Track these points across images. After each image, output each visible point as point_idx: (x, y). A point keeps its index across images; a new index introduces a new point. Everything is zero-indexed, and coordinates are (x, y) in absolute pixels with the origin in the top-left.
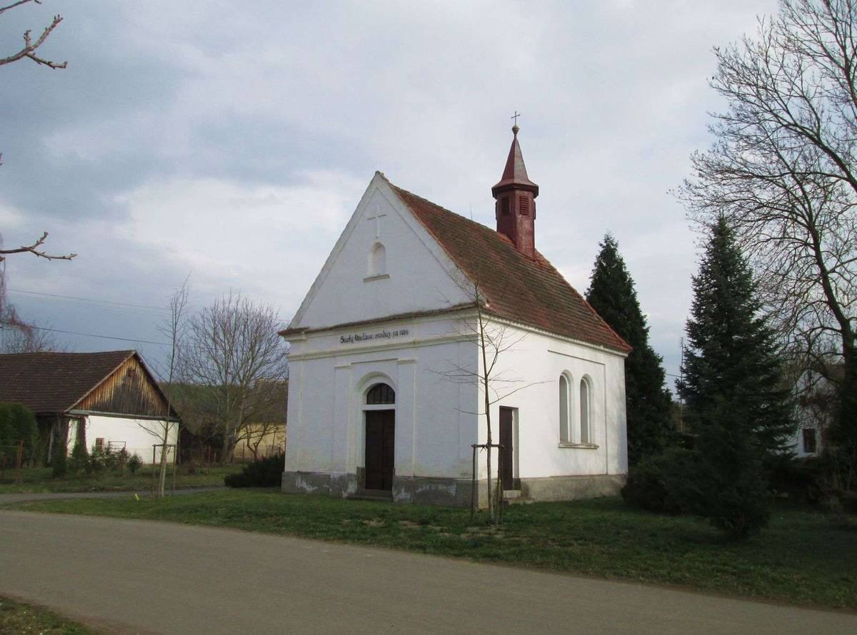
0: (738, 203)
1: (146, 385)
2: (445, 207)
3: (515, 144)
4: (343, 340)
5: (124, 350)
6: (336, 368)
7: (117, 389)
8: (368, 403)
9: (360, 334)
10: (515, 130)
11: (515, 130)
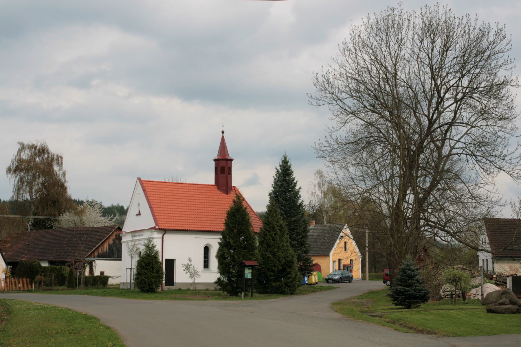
3: (223, 137)
7: (110, 245)
10: (223, 132)
11: (223, 132)
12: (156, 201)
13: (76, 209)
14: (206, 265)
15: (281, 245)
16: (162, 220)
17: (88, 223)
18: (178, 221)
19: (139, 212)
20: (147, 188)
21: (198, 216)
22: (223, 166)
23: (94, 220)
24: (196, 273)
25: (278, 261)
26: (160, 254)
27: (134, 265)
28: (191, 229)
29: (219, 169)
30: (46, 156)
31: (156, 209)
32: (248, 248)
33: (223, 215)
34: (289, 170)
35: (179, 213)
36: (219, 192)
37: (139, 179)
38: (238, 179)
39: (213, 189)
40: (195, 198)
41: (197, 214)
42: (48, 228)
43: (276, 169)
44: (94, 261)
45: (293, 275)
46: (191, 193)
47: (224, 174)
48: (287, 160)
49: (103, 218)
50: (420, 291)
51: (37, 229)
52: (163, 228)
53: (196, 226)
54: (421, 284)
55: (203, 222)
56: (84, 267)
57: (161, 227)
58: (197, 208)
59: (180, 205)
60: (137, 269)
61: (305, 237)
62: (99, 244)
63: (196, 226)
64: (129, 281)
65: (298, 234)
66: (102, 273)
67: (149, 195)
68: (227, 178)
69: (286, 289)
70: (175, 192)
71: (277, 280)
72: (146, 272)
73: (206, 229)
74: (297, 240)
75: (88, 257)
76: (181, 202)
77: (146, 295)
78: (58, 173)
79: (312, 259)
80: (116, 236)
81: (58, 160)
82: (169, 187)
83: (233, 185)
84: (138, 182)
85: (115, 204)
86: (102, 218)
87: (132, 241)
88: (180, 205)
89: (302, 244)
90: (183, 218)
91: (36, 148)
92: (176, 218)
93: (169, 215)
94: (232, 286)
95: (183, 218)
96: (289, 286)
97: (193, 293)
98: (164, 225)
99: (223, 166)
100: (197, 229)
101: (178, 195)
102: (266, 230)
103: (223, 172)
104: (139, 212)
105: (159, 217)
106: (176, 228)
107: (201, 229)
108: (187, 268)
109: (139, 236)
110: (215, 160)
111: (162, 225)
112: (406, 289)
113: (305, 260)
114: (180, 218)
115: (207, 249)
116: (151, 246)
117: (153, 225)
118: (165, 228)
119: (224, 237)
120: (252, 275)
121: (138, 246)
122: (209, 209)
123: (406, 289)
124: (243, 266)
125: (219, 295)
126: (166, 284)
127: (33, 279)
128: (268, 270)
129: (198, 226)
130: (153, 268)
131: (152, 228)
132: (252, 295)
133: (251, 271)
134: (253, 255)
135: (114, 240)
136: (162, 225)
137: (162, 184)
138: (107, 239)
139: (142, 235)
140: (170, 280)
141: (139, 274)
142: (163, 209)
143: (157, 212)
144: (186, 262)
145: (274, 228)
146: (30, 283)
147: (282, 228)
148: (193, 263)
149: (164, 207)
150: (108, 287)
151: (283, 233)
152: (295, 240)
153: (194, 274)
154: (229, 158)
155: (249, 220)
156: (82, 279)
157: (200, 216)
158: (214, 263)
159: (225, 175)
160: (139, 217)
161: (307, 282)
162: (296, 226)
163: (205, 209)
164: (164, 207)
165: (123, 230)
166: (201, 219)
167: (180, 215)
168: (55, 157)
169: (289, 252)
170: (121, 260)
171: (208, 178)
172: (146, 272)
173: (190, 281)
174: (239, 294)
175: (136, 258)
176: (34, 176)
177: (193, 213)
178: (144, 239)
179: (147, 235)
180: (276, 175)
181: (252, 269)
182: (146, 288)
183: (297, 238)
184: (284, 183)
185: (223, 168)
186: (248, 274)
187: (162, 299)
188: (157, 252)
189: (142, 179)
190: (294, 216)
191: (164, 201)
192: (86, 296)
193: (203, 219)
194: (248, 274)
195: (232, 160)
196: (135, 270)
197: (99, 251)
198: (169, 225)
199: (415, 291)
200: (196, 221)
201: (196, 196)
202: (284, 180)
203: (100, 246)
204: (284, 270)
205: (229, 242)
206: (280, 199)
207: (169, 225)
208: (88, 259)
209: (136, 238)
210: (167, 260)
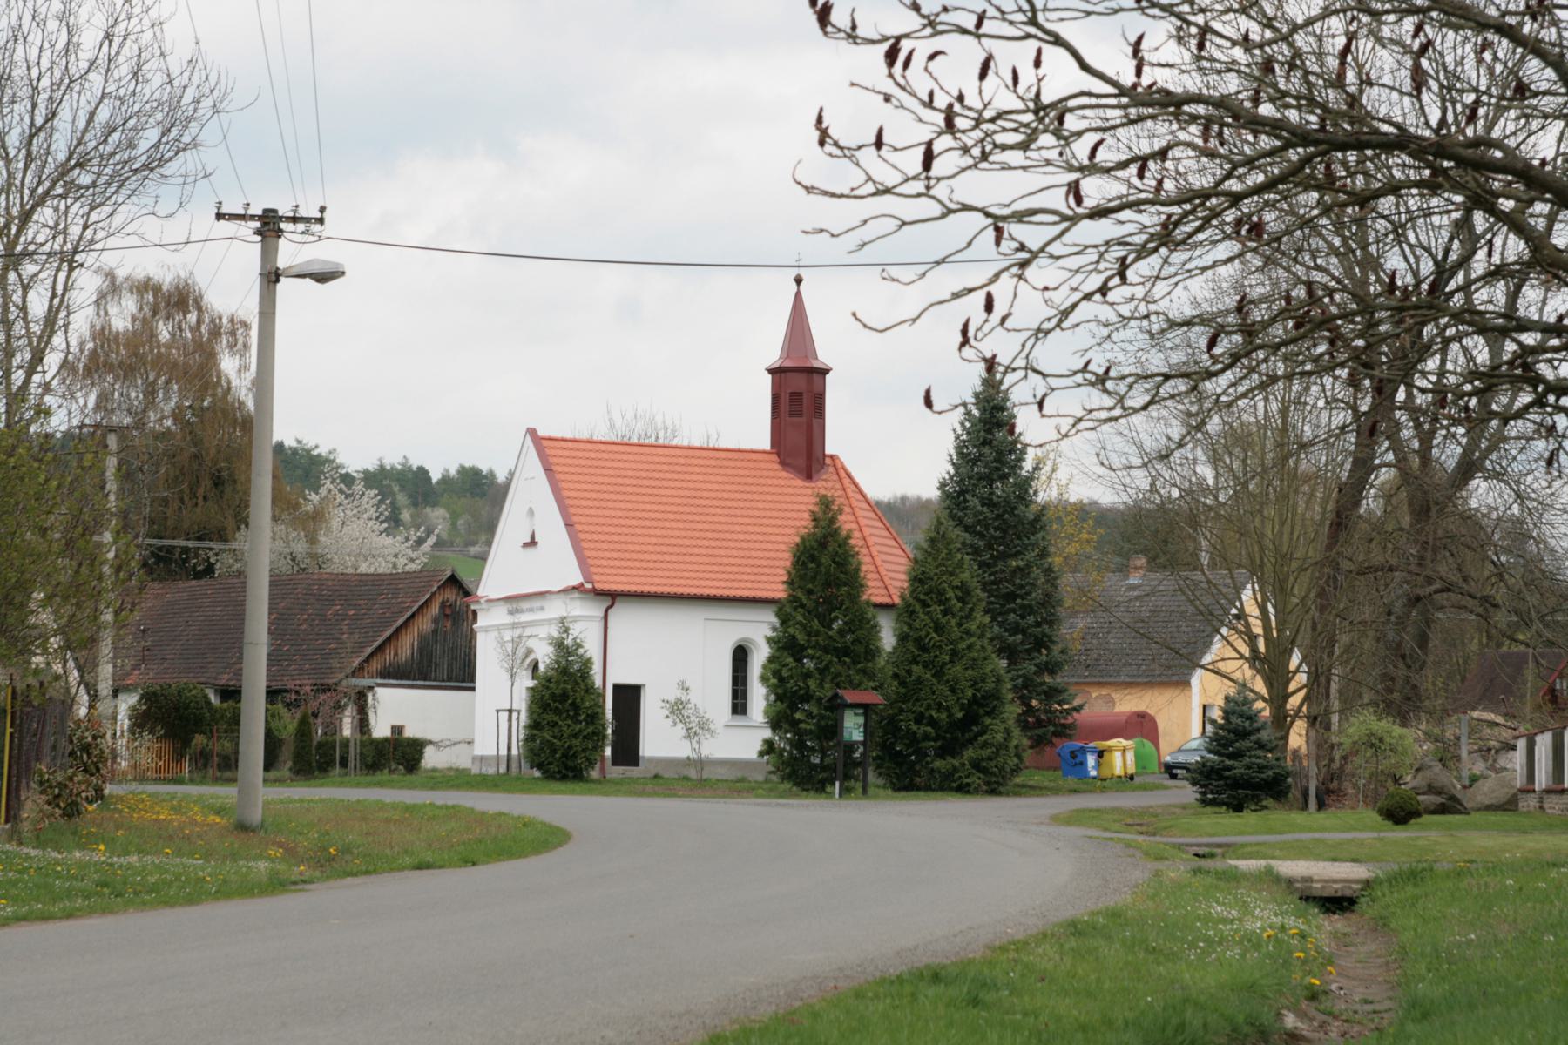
0: (435, 609)
3: (798, 294)
12: (584, 503)
13: (297, 506)
14: (739, 705)
15: (962, 645)
16: (604, 563)
17: (336, 559)
18: (651, 565)
19: (533, 536)
20: (555, 460)
21: (716, 552)
22: (799, 392)
23: (362, 544)
24: (704, 725)
25: (953, 690)
26: (596, 670)
27: (521, 702)
28: (693, 591)
29: (785, 399)
30: (192, 318)
31: (585, 528)
32: (859, 649)
33: (781, 555)
34: (1002, 409)
35: (654, 540)
36: (784, 474)
37: (532, 432)
38: (844, 431)
39: (763, 465)
40: (706, 494)
41: (713, 543)
42: (198, 575)
44: (371, 688)
45: (999, 737)
46: (694, 477)
47: (800, 415)
49: (389, 540)
50: (1261, 769)
51: (162, 580)
52: (606, 587)
53: (709, 583)
54: (1270, 751)
55: (729, 569)
56: (339, 707)
57: (599, 586)
58: (713, 527)
59: (659, 516)
60: (531, 711)
61: (1052, 621)
62: (388, 633)
63: (709, 583)
64: (503, 752)
65: (1027, 610)
66: (397, 730)
67: (563, 485)
68: (810, 428)
69: (975, 779)
70: (643, 474)
71: (946, 751)
72: (556, 718)
73: (738, 593)
74: (1023, 632)
75: (354, 674)
76: (662, 508)
78: (235, 383)
79: (1072, 690)
81: (233, 333)
82: (625, 457)
84: (529, 441)
85: (393, 460)
86: (386, 541)
87: (514, 626)
88: (659, 516)
89: (1041, 643)
90: (667, 558)
91: (157, 289)
92: (647, 557)
93: (624, 547)
94: (807, 760)
95: (667, 558)
96: (984, 771)
97: (694, 779)
98: (611, 579)
99: (799, 392)
100: (713, 592)
101: (653, 483)
102: (916, 598)
103: (796, 410)
104: (533, 536)
105: (594, 554)
106: (647, 589)
107: (725, 593)
108: (677, 709)
109: (531, 610)
110: (772, 371)
111: (603, 578)
112: (1228, 762)
113: (1045, 693)
114: (660, 557)
115: (741, 656)
116: (569, 642)
117: (576, 578)
118: (613, 587)
119: (785, 620)
120: (865, 732)
121: (531, 643)
122: (750, 529)
123: (1228, 762)
124: (836, 706)
126: (616, 761)
127: (186, 743)
128: (919, 720)
129: (717, 584)
130: (575, 707)
132: (865, 791)
133: (861, 720)
134: (871, 676)
135: (435, 620)
136: (603, 578)
137: (602, 447)
138: (413, 616)
139: (542, 609)
140: (628, 751)
141: (535, 726)
142: (605, 529)
143: (589, 537)
144: (674, 694)
145: (941, 593)
146: (179, 757)
147: (968, 593)
148: (694, 697)
149: (609, 521)
151: (972, 610)
152: (1015, 629)
153: (697, 728)
154: (816, 364)
155: (858, 570)
156: (352, 750)
157: (722, 552)
158: (758, 696)
159: (803, 420)
160: (530, 551)
161: (1093, 773)
162: (1022, 587)
163: (737, 528)
164: (609, 521)
165: (480, 593)
166: (726, 561)
167: (658, 549)
168: (225, 321)
169: (990, 667)
170: (473, 689)
171: (752, 428)
172: (556, 718)
174: (829, 789)
175: (526, 682)
176: (150, 392)
177: (699, 542)
178: (549, 622)
179: (556, 609)
180: (962, 424)
181: (866, 715)
182: (553, 768)
183: (1023, 623)
184: (986, 450)
185: (796, 397)
186: (853, 728)
187: (606, 794)
188: (587, 663)
189: (541, 433)
190: (1016, 555)
191: (610, 505)
193: (733, 561)
194: (853, 728)
195: (824, 372)
196: (524, 716)
197: (389, 656)
198: (624, 579)
199: (1248, 767)
200: (710, 568)
201: (709, 486)
202: (985, 443)
203: (389, 639)
204: (971, 719)
206: (974, 502)
207: (624, 579)
209: (524, 618)
210: (618, 688)
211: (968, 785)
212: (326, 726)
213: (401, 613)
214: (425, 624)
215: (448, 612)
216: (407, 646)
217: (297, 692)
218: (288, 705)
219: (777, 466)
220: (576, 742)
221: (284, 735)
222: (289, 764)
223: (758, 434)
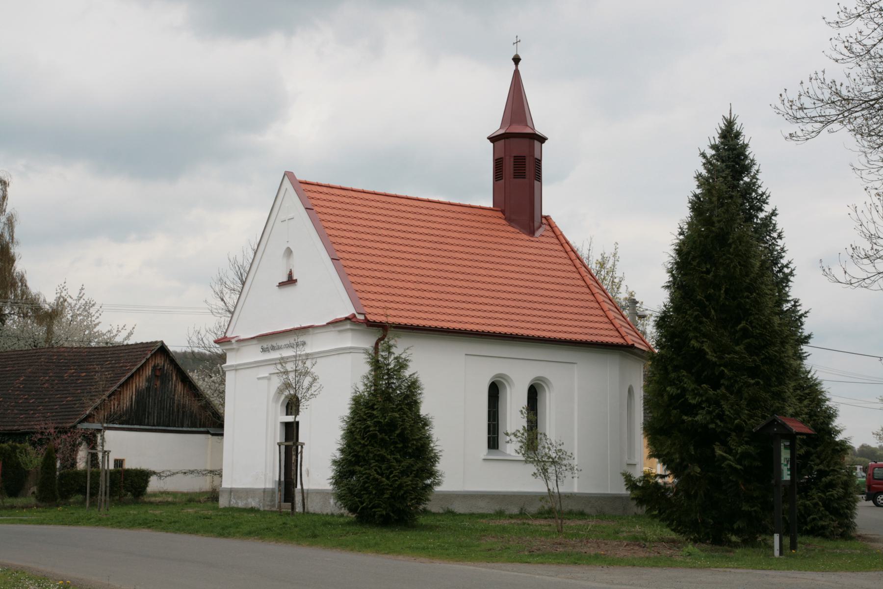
0: (148, 372)
1: (180, 387)
2: (144, 341)
3: (517, 73)
4: (264, 350)
5: (149, 341)
6: (259, 379)
7: (139, 393)
8: (287, 414)
9: (274, 343)
10: (517, 60)
11: (517, 60)
19: (290, 275)
22: (518, 155)
36: (512, 229)
37: (289, 175)
39: (490, 220)
43: (703, 155)
48: (736, 127)
56: (74, 448)
72: (383, 452)
75: (85, 420)
77: (373, 534)
80: (154, 368)
83: (544, 213)
84: (287, 184)
99: (518, 155)
104: (290, 275)
110: (493, 139)
115: (495, 391)
117: (347, 310)
125: (638, 541)
131: (347, 319)
135: (149, 380)
138: (132, 376)
150: (146, 499)
160: (289, 290)
172: (383, 452)
173: (538, 486)
192: (145, 533)
195: (542, 140)
205: (701, 353)
208: (85, 425)
211: (823, 527)
212: (63, 460)
213: (123, 374)
214: (141, 383)
215: (158, 374)
216: (128, 398)
217: (42, 433)
218: (33, 444)
219: (504, 222)
220: (407, 480)
221: (31, 468)
222: (34, 489)
223: (483, 197)
